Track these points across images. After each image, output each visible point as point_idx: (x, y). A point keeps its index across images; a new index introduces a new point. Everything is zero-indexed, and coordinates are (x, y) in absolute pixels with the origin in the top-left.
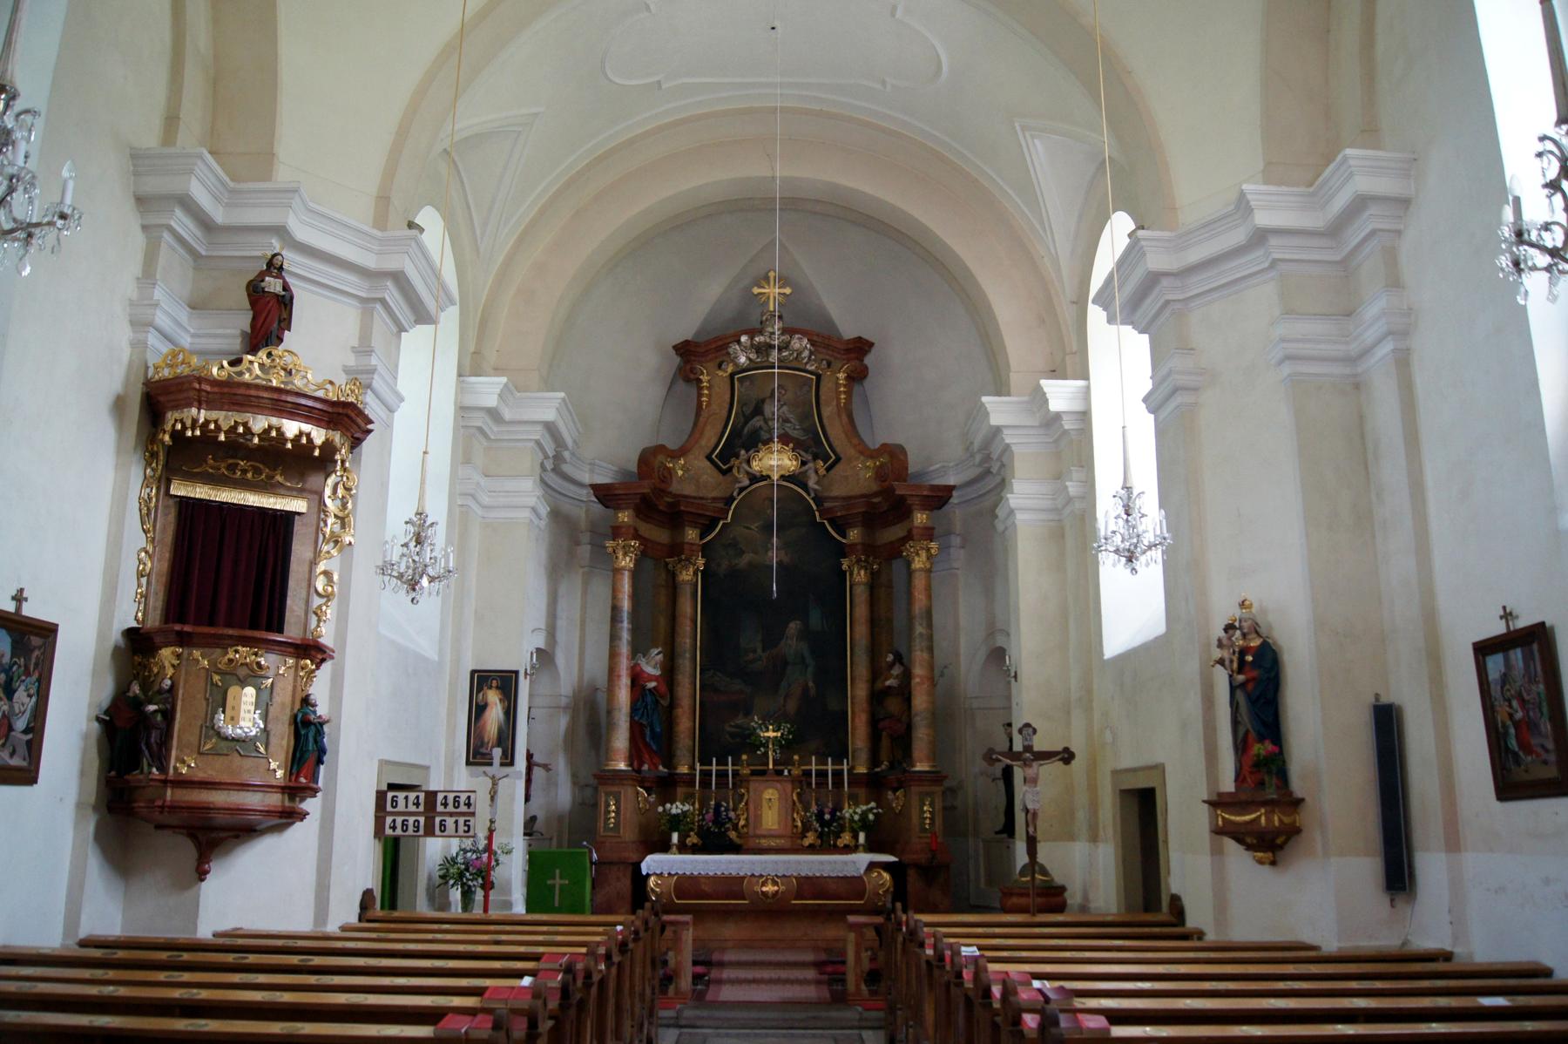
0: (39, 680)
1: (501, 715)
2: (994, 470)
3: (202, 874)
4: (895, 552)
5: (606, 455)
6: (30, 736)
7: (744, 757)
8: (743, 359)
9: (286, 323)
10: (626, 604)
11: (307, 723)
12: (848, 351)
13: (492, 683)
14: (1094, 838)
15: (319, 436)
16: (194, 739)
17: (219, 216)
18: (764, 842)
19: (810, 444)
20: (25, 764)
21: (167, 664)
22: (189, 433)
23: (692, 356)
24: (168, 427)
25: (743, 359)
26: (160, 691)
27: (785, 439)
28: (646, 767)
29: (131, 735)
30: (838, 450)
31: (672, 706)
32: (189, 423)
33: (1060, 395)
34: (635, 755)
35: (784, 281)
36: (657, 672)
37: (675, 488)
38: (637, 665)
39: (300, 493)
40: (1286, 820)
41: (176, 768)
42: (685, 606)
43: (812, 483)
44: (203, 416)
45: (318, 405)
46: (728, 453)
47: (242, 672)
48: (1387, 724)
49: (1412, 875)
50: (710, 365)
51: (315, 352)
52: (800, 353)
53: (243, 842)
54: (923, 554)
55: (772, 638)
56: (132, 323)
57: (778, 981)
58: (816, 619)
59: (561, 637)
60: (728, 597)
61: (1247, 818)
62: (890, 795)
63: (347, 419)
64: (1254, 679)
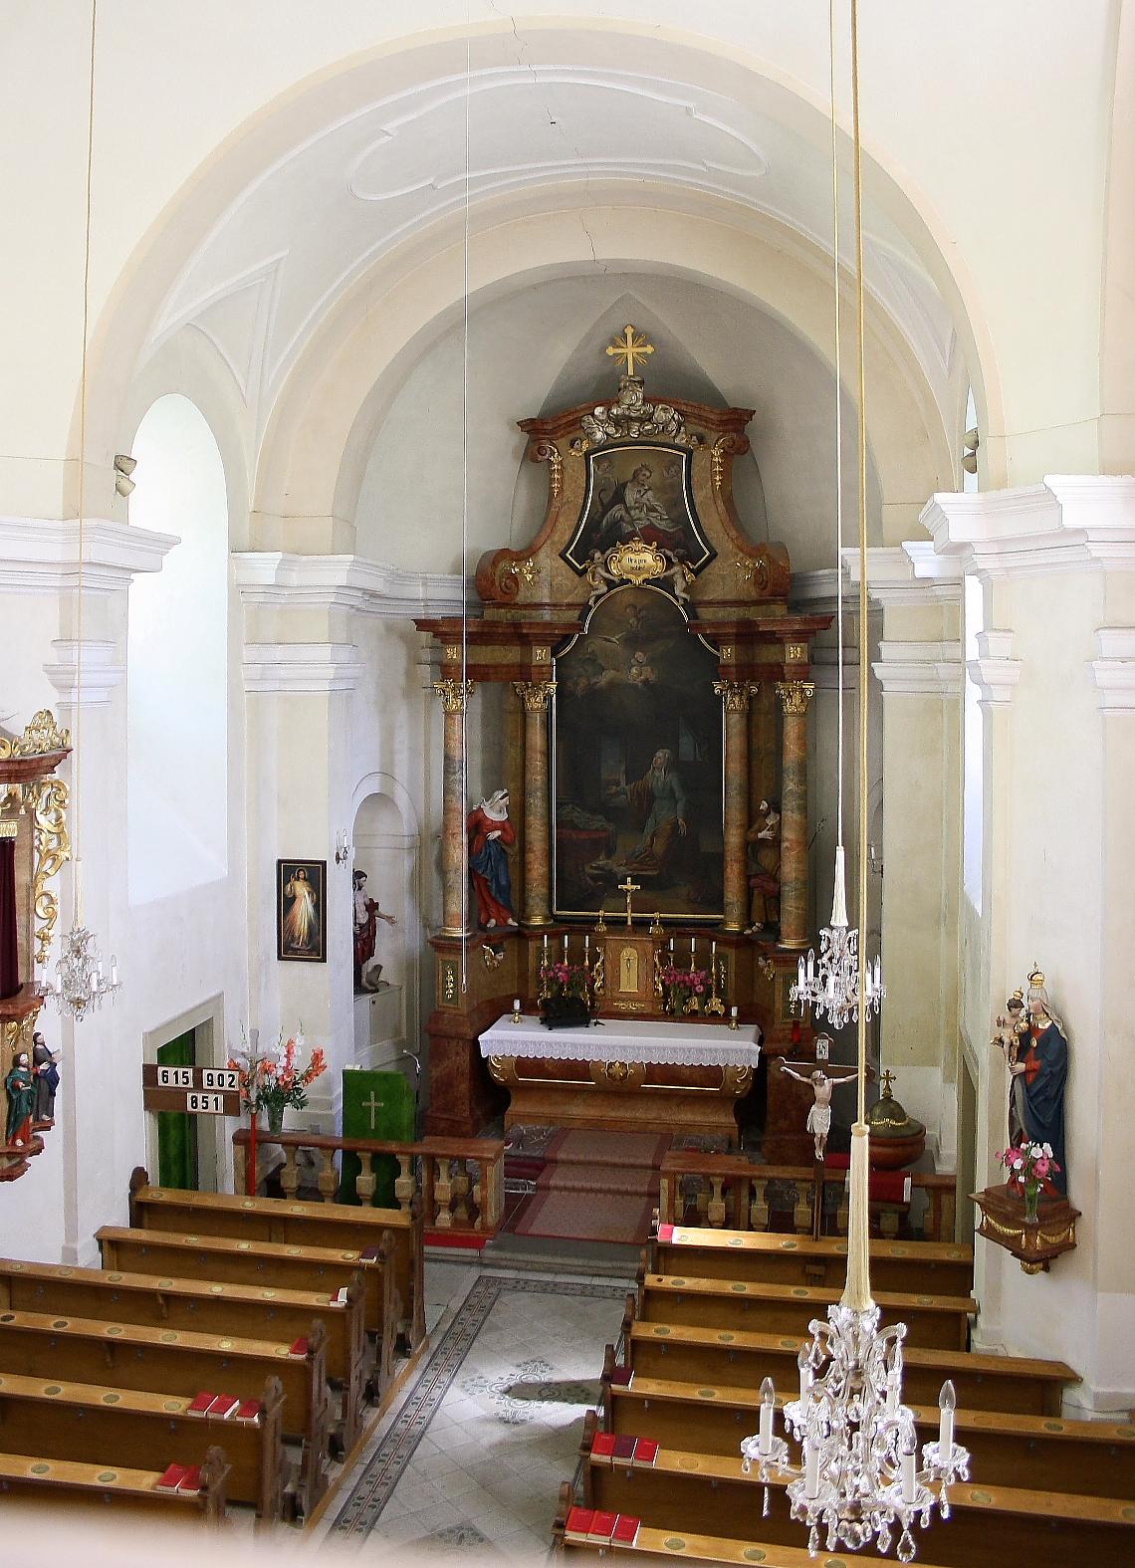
1: (311, 909)
8: (599, 435)
12: (723, 423)
13: (300, 875)
18: (622, 1006)
19: (680, 545)
23: (543, 432)
25: (599, 435)
30: (713, 543)
31: (524, 850)
42: (536, 738)
46: (583, 554)
50: (563, 442)
52: (666, 425)
55: (637, 769)
58: (687, 745)
59: (402, 771)
60: (583, 722)
64: (1034, 1070)
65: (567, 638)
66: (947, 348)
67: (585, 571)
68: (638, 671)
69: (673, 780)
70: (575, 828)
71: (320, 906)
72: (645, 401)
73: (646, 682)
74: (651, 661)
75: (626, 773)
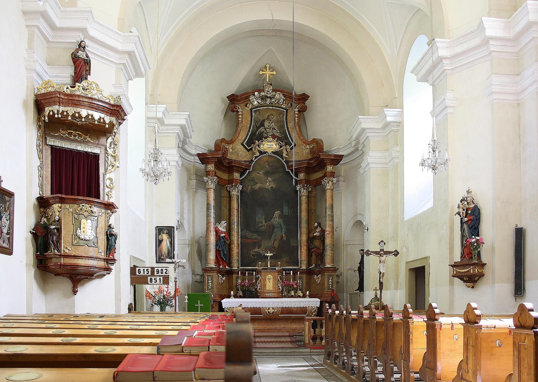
0: (9, 214)
2: (360, 149)
3: (75, 292)
4: (318, 183)
5: (203, 140)
6: (8, 236)
7: (260, 263)
9: (88, 72)
10: (212, 203)
11: (112, 235)
13: (165, 232)
14: (396, 288)
15: (108, 119)
16: (70, 240)
17: (58, 23)
19: (284, 139)
20: (8, 246)
21: (56, 210)
22: (56, 116)
23: (235, 101)
24: (47, 114)
26: (55, 221)
27: (274, 137)
28: (221, 267)
29: (45, 238)
32: (56, 112)
33: (390, 115)
34: (217, 262)
35: (272, 69)
36: (224, 230)
37: (229, 156)
38: (217, 227)
39: (98, 145)
40: (480, 271)
41: (64, 251)
42: (235, 205)
43: (284, 155)
44: (61, 109)
45: (107, 106)
46: (251, 142)
47: (86, 214)
48: (520, 234)
49: (524, 289)
50: (243, 105)
51: (103, 81)
53: (87, 282)
54: (330, 183)
55: (268, 218)
56: (26, 69)
57: (277, 342)
58: (286, 210)
59: (186, 216)
61: (466, 270)
62: (315, 277)
63: (117, 111)
64: (471, 219)
65: (245, 170)
66: (399, 45)
67: (251, 149)
68: (269, 184)
69: (281, 221)
70: (247, 238)
71: (172, 243)
72: (273, 90)
73: (272, 188)
74: (274, 181)
75: (265, 219)
